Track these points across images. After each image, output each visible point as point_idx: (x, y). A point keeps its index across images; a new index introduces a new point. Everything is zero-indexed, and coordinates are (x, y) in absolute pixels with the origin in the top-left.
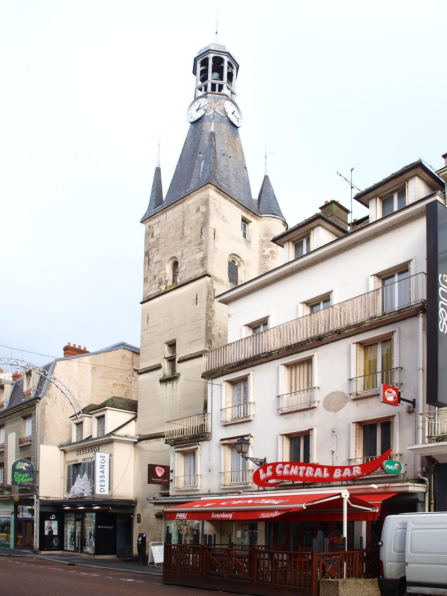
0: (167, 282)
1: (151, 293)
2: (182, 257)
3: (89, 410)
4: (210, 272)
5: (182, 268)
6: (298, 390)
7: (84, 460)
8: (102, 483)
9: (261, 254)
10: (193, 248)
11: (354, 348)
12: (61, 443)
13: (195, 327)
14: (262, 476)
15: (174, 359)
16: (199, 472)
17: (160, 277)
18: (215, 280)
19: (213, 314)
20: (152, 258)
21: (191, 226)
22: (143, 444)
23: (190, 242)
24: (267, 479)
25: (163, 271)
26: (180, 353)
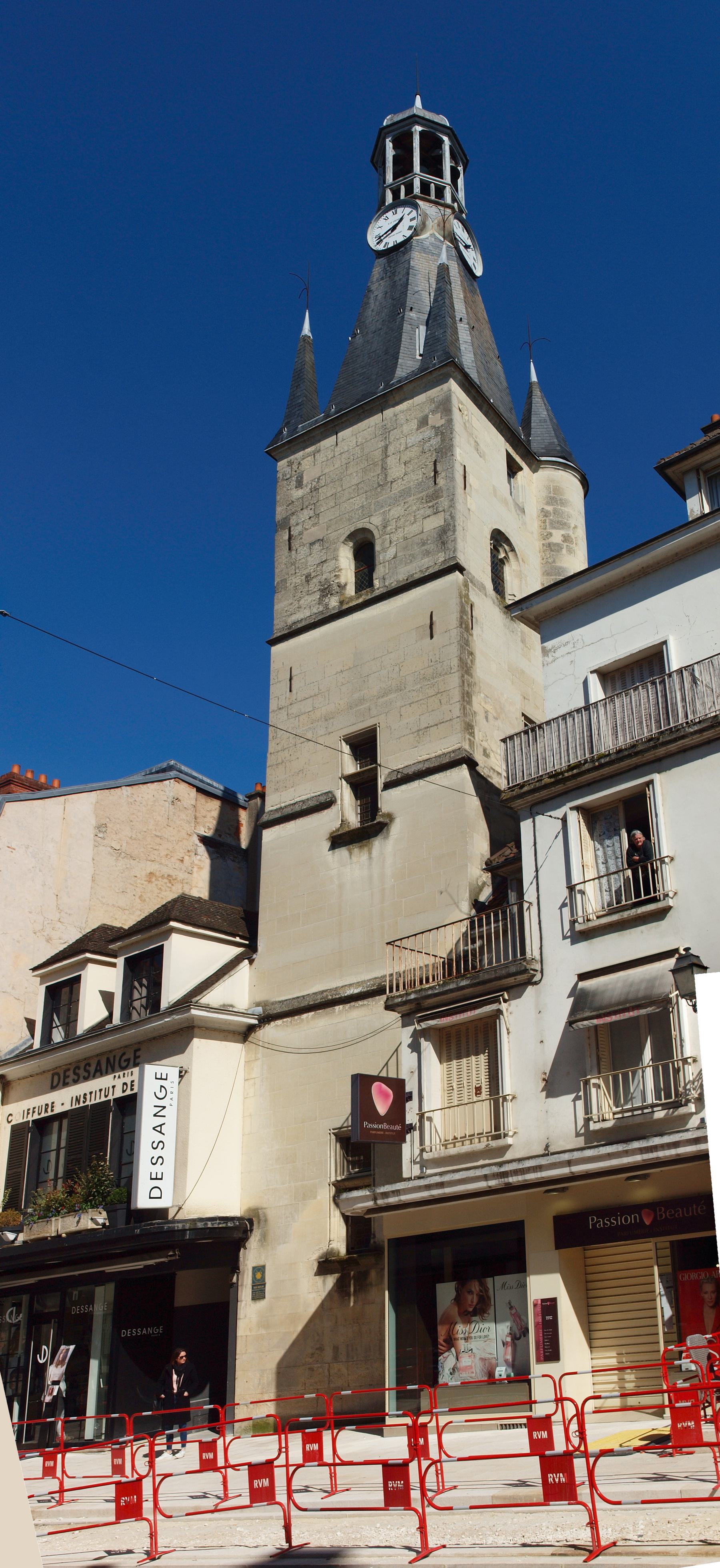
0: (342, 587)
2: (385, 527)
3: (99, 942)
5: (384, 554)
7: (78, 1100)
8: (157, 1169)
9: (544, 542)
11: (575, 820)
13: (431, 692)
16: (508, 1086)
17: (324, 577)
18: (472, 582)
19: (472, 661)
20: (301, 533)
21: (405, 458)
22: (270, 1032)
23: (406, 493)
26: (392, 758)
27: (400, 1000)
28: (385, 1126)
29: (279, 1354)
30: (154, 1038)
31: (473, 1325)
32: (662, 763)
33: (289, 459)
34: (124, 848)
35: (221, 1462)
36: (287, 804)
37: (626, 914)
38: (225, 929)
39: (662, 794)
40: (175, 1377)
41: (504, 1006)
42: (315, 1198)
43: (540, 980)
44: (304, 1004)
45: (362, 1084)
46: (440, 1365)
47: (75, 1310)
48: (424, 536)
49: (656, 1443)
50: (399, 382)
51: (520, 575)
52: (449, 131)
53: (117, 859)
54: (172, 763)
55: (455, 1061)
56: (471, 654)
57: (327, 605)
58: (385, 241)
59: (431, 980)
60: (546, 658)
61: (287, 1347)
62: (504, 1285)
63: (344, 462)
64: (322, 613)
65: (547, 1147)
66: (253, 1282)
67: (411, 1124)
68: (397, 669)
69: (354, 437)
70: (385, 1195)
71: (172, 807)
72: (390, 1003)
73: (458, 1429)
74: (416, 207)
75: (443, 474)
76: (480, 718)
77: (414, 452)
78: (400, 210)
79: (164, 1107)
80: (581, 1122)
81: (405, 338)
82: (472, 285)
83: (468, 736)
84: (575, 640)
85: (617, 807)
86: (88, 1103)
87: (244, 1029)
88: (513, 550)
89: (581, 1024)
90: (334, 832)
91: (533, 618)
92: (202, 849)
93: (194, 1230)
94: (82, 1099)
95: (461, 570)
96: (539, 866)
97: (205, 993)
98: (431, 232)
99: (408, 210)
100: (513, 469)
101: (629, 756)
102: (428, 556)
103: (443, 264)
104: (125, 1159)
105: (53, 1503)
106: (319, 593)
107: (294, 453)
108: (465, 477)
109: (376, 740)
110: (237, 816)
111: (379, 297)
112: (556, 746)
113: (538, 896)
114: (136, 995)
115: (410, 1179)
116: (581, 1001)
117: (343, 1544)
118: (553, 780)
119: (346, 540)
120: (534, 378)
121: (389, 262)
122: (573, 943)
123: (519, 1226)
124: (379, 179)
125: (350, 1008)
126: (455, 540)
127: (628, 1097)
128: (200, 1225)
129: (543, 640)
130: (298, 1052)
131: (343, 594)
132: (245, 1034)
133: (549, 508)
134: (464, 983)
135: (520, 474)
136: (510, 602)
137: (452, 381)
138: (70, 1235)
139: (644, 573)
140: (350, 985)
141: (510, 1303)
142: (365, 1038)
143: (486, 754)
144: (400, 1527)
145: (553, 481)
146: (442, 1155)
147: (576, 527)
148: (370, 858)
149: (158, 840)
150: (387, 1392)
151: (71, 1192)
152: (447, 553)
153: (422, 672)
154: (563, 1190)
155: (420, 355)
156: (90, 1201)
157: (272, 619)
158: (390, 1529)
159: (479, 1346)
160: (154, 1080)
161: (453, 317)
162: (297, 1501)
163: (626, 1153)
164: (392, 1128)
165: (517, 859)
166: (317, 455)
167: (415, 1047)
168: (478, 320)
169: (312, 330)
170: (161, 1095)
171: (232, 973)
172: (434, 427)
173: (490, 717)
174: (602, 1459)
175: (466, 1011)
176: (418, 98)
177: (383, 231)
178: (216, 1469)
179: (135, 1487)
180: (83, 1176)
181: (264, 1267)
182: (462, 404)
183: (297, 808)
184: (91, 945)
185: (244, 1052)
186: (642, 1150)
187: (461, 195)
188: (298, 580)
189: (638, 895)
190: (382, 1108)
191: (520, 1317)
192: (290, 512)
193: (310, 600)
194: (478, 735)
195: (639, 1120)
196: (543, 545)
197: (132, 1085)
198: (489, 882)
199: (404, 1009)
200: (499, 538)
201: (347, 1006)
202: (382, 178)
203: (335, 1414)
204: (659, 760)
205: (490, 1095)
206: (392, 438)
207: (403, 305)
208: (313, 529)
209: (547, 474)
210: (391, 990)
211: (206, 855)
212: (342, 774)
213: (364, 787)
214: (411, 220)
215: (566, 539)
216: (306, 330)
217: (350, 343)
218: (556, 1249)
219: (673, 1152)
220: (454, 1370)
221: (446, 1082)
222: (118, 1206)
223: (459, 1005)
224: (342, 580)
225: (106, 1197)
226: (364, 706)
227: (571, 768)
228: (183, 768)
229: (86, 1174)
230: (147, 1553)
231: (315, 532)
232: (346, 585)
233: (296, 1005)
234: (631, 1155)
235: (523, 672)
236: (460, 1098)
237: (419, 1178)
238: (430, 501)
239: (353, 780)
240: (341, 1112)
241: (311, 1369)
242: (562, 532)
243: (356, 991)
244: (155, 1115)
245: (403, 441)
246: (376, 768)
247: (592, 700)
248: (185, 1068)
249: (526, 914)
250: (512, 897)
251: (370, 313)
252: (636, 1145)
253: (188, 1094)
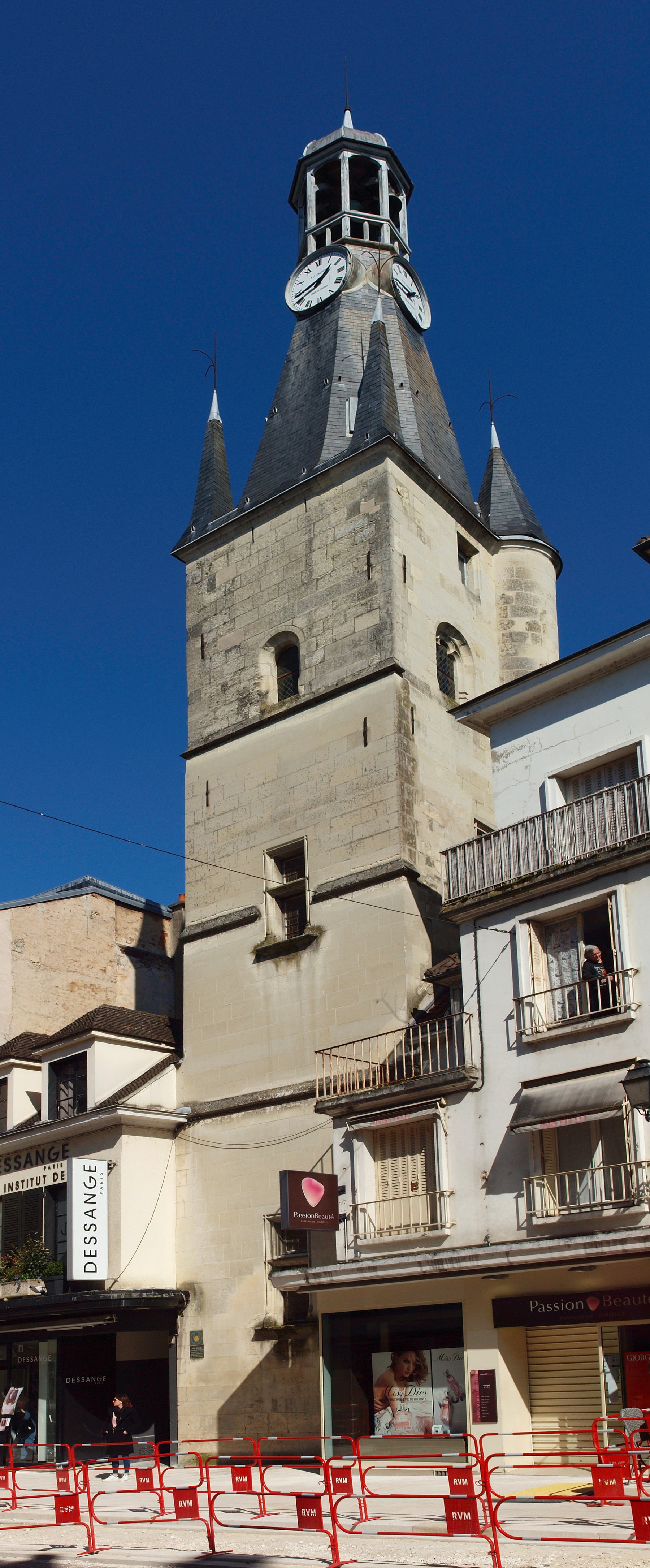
0: (263, 695)
1: (216, 727)
2: (310, 629)
4: (401, 661)
5: (311, 658)
8: (91, 1247)
9: (504, 632)
10: (345, 606)
11: (524, 933)
13: (365, 802)
16: (445, 1182)
17: (243, 685)
18: (413, 683)
19: (413, 768)
21: (332, 552)
22: (200, 1129)
23: (335, 590)
25: (251, 672)
26: (319, 873)
27: (330, 1104)
29: (221, 1403)
30: (83, 1134)
31: (410, 1389)
32: (626, 874)
33: (199, 560)
34: (43, 961)
35: (156, 1485)
36: (208, 919)
37: (580, 1027)
38: (150, 1036)
39: (627, 905)
40: (114, 1418)
41: (441, 1111)
42: (251, 1273)
43: (481, 1087)
45: (291, 1181)
46: (376, 1420)
47: (21, 1360)
48: (356, 637)
49: (586, 1495)
50: (325, 466)
51: (473, 671)
52: (386, 153)
53: (37, 972)
54: (88, 878)
55: (389, 1160)
56: (413, 760)
57: (246, 715)
58: (307, 299)
59: (364, 1085)
60: (497, 764)
61: (227, 1398)
62: (441, 1357)
63: (262, 560)
64: (241, 723)
65: (487, 1238)
66: (191, 1344)
67: (345, 1215)
68: (326, 779)
69: (273, 532)
70: (317, 1275)
71: (90, 921)
72: (320, 1106)
73: (382, 1473)
74: (344, 253)
75: (378, 567)
76: (423, 828)
77: (345, 543)
78: (325, 260)
79: (95, 1195)
80: (523, 1217)
81: (332, 412)
82: (417, 341)
83: (407, 847)
84: (531, 743)
85: (575, 919)
86: (20, 1189)
87: (173, 1127)
88: (465, 644)
89: (522, 1129)
90: (258, 945)
91: (481, 721)
92: (125, 959)
93: (129, 1299)
94: (14, 1186)
95: (400, 671)
96: (480, 979)
97: (131, 1095)
98: (364, 282)
99: (335, 258)
100: (465, 553)
101: (589, 867)
102: (360, 658)
103: (378, 322)
104: (60, 1238)
105: (8, 1507)
106: (237, 703)
107: (205, 554)
108: (405, 569)
109: (303, 853)
110: (162, 926)
111: (301, 367)
112: (504, 857)
113: (480, 1007)
114: (63, 1096)
115: (344, 1262)
116: (524, 1108)
117: (264, 1554)
118: (500, 893)
119: (266, 645)
120: (496, 443)
121: (312, 325)
122: (519, 1054)
123: (457, 1307)
124: (300, 223)
125: (282, 1109)
126: (392, 640)
127: (575, 1196)
128: (135, 1296)
129: (494, 744)
130: (228, 1147)
131: (265, 703)
132: (175, 1131)
133: (512, 594)
134: (398, 1089)
135: (475, 558)
136: (461, 702)
137: (388, 461)
138: (11, 1299)
139: (617, 667)
140: (281, 1088)
141: (447, 1372)
142: (298, 1136)
144: (316, 1544)
145: (516, 562)
146: (377, 1242)
147: (544, 612)
148: (299, 970)
150: (323, 1440)
151: (10, 1264)
152: (384, 654)
153: (355, 782)
155: (351, 432)
156: (28, 1272)
157: (187, 733)
158: (312, 1546)
159: (418, 1406)
160: (83, 1172)
161: (391, 385)
162: (219, 1519)
163: (569, 1247)
164: (324, 1217)
165: (457, 971)
166: (231, 555)
167: (347, 1146)
168: (423, 382)
169: (221, 413)
171: (158, 1076)
172: (368, 515)
174: (503, 1505)
175: (401, 1114)
176: (348, 113)
177: (303, 289)
178: (152, 1490)
179: (73, 1499)
180: (20, 1252)
181: (201, 1332)
182: (401, 485)
183: (219, 923)
184: (14, 1052)
185: (174, 1147)
186: (585, 1246)
187: (404, 232)
188: (212, 690)
189: (595, 1007)
191: (457, 1385)
192: (202, 618)
193: (227, 710)
194: (420, 845)
195: (584, 1217)
196: (503, 635)
197: (62, 1176)
198: (431, 991)
199: (336, 1112)
200: (447, 633)
201: (279, 1107)
202: (303, 221)
203: (262, 1454)
204: (624, 869)
205: (427, 1190)
206: (317, 530)
207: (330, 376)
208: (228, 635)
209: (509, 555)
210: (321, 1094)
211: (130, 964)
212: (267, 888)
213: (291, 901)
214: (339, 271)
215: (532, 626)
216: (215, 413)
217: (267, 424)
218: (496, 1326)
219: (619, 1248)
220: (390, 1425)
221: (380, 1178)
222: (55, 1278)
223: (396, 1108)
224: (263, 688)
225: (43, 1269)
226: (290, 818)
227: (521, 880)
228: (100, 883)
229: (23, 1249)
230: (87, 1549)
231: (231, 638)
232: (267, 692)
233: (225, 1106)
234: (576, 1248)
235: (475, 775)
236: (395, 1191)
237: (354, 1261)
238: (363, 598)
239: (279, 894)
240: (272, 1202)
241: (251, 1417)
242: (527, 619)
243: (288, 1094)
244: (85, 1202)
245: (330, 533)
246: (304, 881)
247: (550, 807)
248: (114, 1161)
249: (466, 1026)
250: (454, 1006)
251: (290, 387)
252: (579, 1240)
253: (118, 1184)
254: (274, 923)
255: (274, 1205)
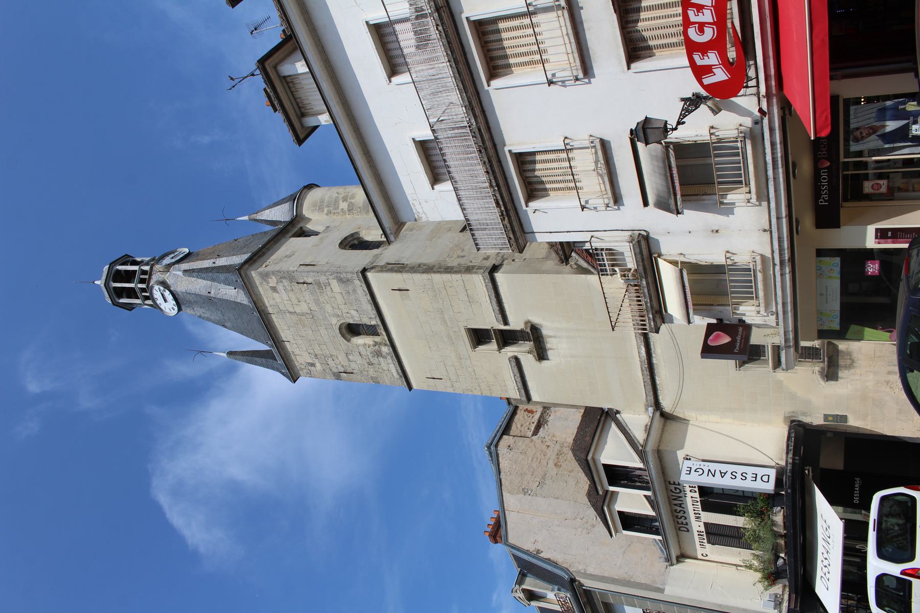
0: (376, 344)
3: (600, 501)
6: (535, 48)
8: (749, 477)
12: (663, 560)
14: (720, 75)
15: (501, 331)
20: (343, 366)
21: (296, 302)
23: (317, 302)
24: (726, 63)
25: (361, 349)
26: (489, 321)
28: (739, 338)
42: (782, 381)
44: (649, 382)
45: (708, 351)
48: (344, 292)
76: (462, 261)
77: (291, 294)
78: (155, 296)
87: (662, 419)
120: (246, 218)
133: (326, 210)
134: (644, 282)
143: (487, 258)
148: (555, 337)
149: (535, 460)
154: (797, 222)
160: (691, 477)
170: (701, 472)
173: (462, 254)
183: (519, 379)
190: (726, 339)
199: (658, 321)
210: (645, 329)
213: (507, 338)
215: (345, 199)
218: (839, 227)
224: (371, 343)
231: (342, 358)
233: (650, 387)
240: (727, 365)
252: (770, 173)
254: (522, 350)
255: (731, 363)
